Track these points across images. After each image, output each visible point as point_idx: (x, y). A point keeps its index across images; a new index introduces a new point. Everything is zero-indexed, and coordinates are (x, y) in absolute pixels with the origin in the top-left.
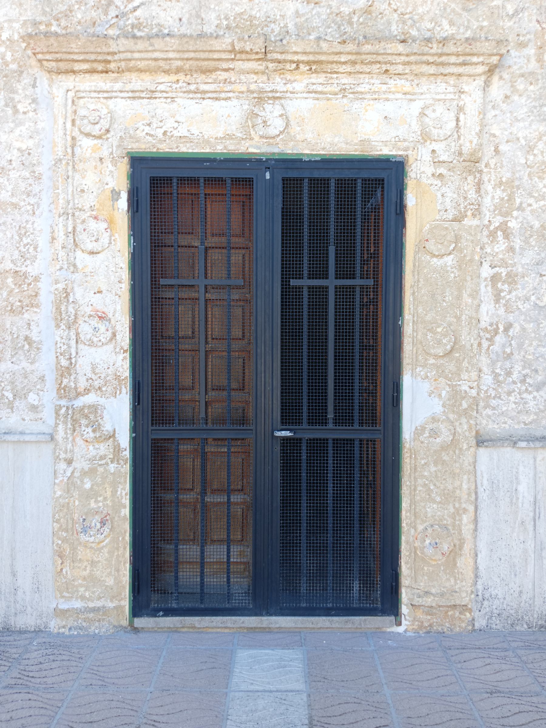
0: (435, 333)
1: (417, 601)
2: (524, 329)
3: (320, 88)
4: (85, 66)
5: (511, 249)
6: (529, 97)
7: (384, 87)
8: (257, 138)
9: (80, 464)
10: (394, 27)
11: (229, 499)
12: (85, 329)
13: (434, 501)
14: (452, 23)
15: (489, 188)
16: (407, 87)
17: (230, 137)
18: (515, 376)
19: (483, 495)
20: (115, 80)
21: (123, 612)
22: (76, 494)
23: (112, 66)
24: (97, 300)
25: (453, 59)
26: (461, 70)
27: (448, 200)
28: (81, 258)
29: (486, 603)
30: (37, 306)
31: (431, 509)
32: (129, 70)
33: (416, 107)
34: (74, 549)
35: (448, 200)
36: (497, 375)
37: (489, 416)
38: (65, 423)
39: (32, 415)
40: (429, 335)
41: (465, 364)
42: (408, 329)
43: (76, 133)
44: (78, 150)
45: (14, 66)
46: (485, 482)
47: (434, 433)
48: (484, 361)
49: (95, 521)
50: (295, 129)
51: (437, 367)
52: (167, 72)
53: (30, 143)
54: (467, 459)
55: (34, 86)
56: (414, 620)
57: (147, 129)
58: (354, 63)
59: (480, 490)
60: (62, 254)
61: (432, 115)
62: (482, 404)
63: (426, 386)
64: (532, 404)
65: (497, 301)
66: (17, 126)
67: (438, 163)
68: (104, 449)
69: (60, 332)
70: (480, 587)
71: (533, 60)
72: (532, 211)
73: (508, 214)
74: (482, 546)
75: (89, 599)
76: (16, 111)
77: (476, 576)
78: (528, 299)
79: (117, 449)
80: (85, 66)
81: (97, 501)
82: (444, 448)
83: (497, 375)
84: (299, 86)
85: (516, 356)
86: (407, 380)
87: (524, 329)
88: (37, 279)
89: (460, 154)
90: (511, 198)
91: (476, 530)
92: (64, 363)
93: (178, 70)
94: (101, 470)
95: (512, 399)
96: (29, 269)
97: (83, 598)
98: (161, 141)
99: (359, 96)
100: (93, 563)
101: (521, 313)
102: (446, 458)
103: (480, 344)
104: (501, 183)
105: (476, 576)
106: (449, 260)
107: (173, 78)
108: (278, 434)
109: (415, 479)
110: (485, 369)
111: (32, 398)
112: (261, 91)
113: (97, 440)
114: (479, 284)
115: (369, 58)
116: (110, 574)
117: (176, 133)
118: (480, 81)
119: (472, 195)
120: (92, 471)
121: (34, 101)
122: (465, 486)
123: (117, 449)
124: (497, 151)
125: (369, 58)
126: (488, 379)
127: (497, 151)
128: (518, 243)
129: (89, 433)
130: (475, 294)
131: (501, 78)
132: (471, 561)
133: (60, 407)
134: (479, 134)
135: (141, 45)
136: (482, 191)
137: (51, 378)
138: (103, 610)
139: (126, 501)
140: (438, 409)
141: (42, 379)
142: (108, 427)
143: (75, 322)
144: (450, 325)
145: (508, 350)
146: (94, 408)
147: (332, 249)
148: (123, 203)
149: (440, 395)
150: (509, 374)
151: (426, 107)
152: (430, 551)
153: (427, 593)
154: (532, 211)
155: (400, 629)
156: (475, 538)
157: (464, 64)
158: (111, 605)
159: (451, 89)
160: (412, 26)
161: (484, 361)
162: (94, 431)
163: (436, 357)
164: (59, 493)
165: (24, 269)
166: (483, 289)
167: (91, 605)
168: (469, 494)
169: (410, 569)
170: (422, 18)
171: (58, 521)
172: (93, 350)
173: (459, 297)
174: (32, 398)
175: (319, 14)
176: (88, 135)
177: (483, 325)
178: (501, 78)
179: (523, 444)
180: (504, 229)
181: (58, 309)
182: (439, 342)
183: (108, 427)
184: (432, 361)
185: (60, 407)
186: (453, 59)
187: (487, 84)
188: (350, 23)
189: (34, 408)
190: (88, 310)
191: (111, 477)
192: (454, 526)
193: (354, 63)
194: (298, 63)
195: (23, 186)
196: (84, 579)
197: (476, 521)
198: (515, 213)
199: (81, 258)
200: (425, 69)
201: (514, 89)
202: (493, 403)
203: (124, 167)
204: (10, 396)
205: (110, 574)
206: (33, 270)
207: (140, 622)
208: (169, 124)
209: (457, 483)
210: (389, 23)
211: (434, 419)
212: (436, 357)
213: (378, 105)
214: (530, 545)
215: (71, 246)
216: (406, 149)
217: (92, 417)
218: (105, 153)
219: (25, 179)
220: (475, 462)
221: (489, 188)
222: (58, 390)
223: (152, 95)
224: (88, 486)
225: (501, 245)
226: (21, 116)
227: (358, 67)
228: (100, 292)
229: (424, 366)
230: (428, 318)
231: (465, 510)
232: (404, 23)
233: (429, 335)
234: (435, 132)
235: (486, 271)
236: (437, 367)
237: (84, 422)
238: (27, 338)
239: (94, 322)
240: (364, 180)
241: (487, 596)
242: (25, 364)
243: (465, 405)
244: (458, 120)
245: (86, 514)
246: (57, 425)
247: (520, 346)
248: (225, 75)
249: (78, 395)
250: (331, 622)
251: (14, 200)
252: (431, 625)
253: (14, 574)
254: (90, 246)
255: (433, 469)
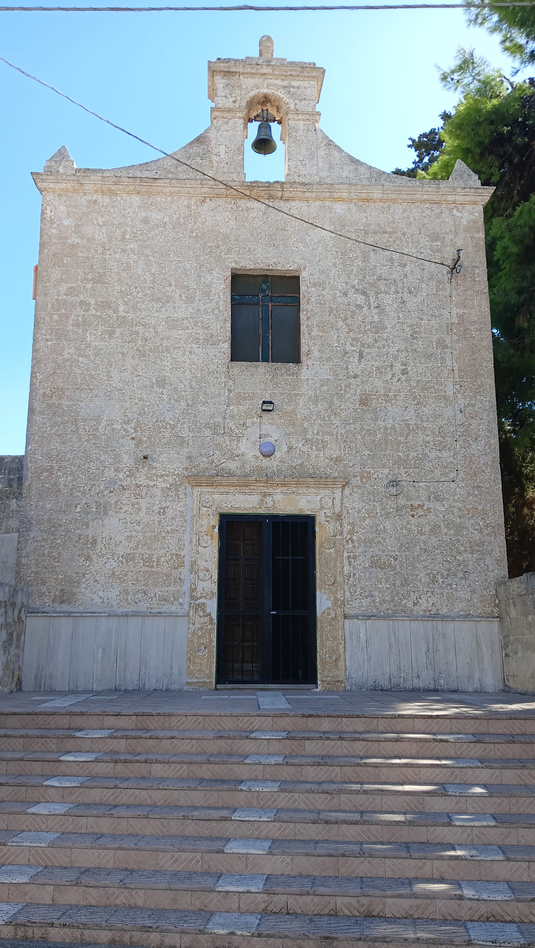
0: (328, 576)
1: (324, 679)
2: (360, 575)
3: (285, 492)
4: (206, 484)
5: (354, 547)
6: (358, 494)
7: (307, 491)
8: (263, 508)
9: (198, 626)
10: (311, 471)
11: (243, 677)
12: (201, 575)
13: (330, 641)
14: (330, 469)
15: (346, 525)
16: (315, 491)
17: (254, 507)
18: (358, 593)
19: (347, 637)
20: (215, 488)
21: (212, 684)
22: (195, 637)
23: (215, 484)
24: (205, 564)
25: (330, 483)
26: (333, 486)
27: (331, 529)
28: (201, 549)
29: (350, 680)
30: (184, 566)
31: (328, 643)
32: (220, 485)
33: (319, 498)
34: (194, 659)
35: (331, 529)
36: (351, 593)
37: (349, 608)
38: (193, 609)
39: (180, 607)
40: (326, 577)
41: (339, 588)
42: (318, 575)
43: (201, 506)
44: (201, 512)
45: (178, 483)
46: (348, 632)
47: (329, 614)
48: (346, 587)
49: (203, 647)
50: (277, 505)
51: (329, 589)
52: (233, 486)
53: (184, 509)
54: (341, 624)
55: (186, 489)
56: (323, 687)
57: (225, 505)
58: (297, 484)
59: (346, 635)
60: (194, 547)
61: (324, 501)
62: (346, 603)
63: (325, 596)
64: (364, 603)
65: (350, 565)
66: (179, 503)
67: (327, 517)
68: (206, 619)
69: (192, 576)
70: (347, 673)
71: (359, 481)
72: (361, 533)
73: (353, 534)
74: (347, 657)
75: (200, 678)
76: (179, 498)
77: (346, 669)
78: (361, 565)
79: (211, 619)
80: (206, 484)
81: (203, 640)
82: (333, 619)
83: (351, 593)
84: (278, 491)
85: (358, 585)
86: (318, 593)
87: (360, 575)
88: (184, 557)
89: (335, 514)
90: (353, 528)
91: (345, 651)
92: (193, 587)
93: (237, 486)
94: (205, 627)
95: (357, 601)
96: (181, 553)
97: (197, 678)
98: (230, 509)
99: (299, 494)
100: (201, 664)
101: (359, 570)
102: (333, 624)
103: (344, 581)
104: (350, 523)
105: (346, 669)
106: (332, 550)
107: (236, 488)
108: (271, 613)
109: (322, 632)
110: (346, 590)
111: (181, 600)
112: (265, 492)
113: (204, 616)
114: (343, 559)
115: (302, 483)
116: (207, 669)
117: (235, 506)
118: (341, 489)
119: (339, 527)
120: (202, 628)
121: (185, 494)
122: (340, 634)
123: (211, 619)
124: (348, 512)
125: (302, 483)
126: (348, 594)
127: (348, 512)
128: (356, 545)
129: (201, 613)
130: (342, 562)
131: (348, 487)
132: (343, 663)
133: (192, 603)
134: (341, 507)
135: (225, 479)
136: (343, 526)
137: (187, 593)
138: (206, 683)
139: (215, 640)
140: (330, 605)
141: (184, 593)
142: (208, 611)
143: (197, 572)
144: (333, 573)
145: (355, 583)
146: (204, 604)
147: (290, 546)
148: (216, 530)
149: (330, 600)
150: (355, 592)
151: (322, 498)
152: (328, 659)
153: (328, 676)
154: (361, 533)
155: (318, 690)
156: (345, 654)
157: (334, 484)
158: (208, 681)
159: (330, 492)
160: (317, 470)
161: (346, 587)
162: (203, 613)
163: (329, 585)
164: (190, 636)
165: (179, 553)
166: (345, 561)
167: (200, 680)
168: (342, 637)
169: (321, 666)
170: (320, 467)
171: (189, 647)
172: (203, 582)
173: (336, 564)
174: (181, 600)
175: (285, 466)
176: (205, 507)
177: (345, 574)
178: (348, 487)
179: (361, 618)
180: (351, 539)
181: (192, 567)
182: (329, 580)
183: (208, 611)
184: (327, 587)
185: (192, 603)
186: (330, 483)
187: (343, 489)
188: (296, 469)
189: (181, 604)
190: (202, 568)
191: (209, 631)
192: (337, 649)
193: (297, 484)
194: (278, 484)
195: (180, 524)
196: (197, 671)
197: (345, 647)
198: (355, 534)
199: (201, 549)
200: (321, 486)
201: (353, 491)
202: (350, 603)
203: (217, 518)
204: (173, 600)
205: (207, 669)
206: (182, 553)
207: (219, 686)
208: (233, 504)
209: (337, 633)
210: (309, 469)
211: (328, 608)
212: (329, 585)
213: (305, 497)
214: (366, 657)
215: (197, 545)
216: (315, 512)
217: (202, 607)
218: (210, 513)
219: (181, 521)
220: (344, 625)
221: (346, 525)
222: (191, 597)
223: (227, 493)
224: (200, 634)
225: (351, 545)
226: (181, 500)
227: (298, 485)
228: (207, 561)
229: (324, 589)
230: (325, 571)
231: (341, 643)
232: (314, 469)
233: (326, 577)
234: (325, 506)
235: (345, 555)
236: (329, 589)
237: (200, 609)
238: (179, 578)
239: (204, 572)
240: (301, 522)
241: (350, 677)
242: (178, 588)
243: (339, 603)
244: (333, 502)
245: (199, 644)
246: (190, 610)
247: (359, 582)
248: (253, 487)
249: (198, 599)
250: (291, 686)
251: (177, 529)
252: (329, 689)
253: (171, 668)
254: (204, 545)
255: (329, 628)
